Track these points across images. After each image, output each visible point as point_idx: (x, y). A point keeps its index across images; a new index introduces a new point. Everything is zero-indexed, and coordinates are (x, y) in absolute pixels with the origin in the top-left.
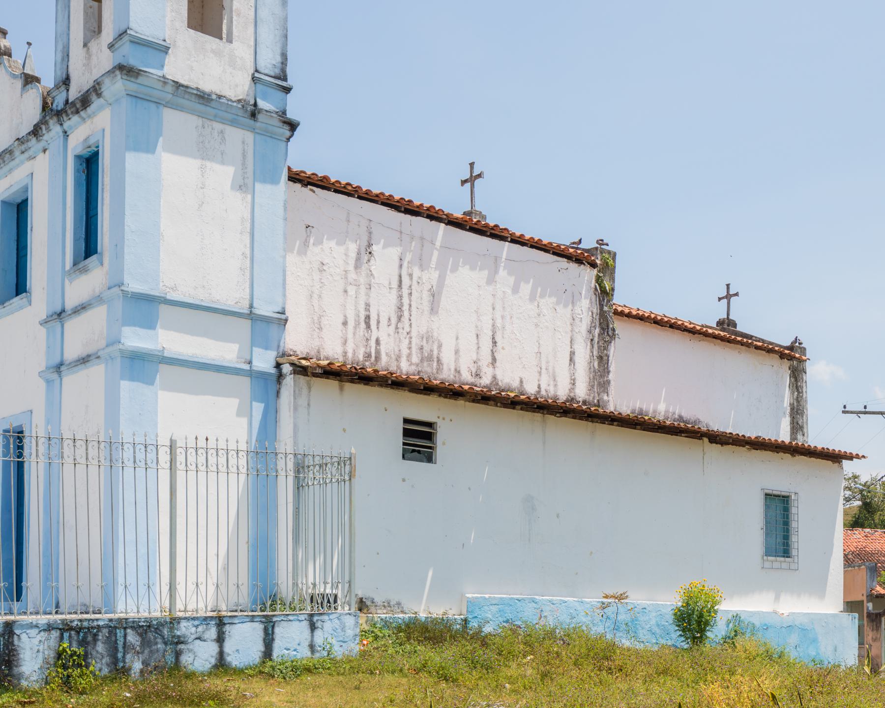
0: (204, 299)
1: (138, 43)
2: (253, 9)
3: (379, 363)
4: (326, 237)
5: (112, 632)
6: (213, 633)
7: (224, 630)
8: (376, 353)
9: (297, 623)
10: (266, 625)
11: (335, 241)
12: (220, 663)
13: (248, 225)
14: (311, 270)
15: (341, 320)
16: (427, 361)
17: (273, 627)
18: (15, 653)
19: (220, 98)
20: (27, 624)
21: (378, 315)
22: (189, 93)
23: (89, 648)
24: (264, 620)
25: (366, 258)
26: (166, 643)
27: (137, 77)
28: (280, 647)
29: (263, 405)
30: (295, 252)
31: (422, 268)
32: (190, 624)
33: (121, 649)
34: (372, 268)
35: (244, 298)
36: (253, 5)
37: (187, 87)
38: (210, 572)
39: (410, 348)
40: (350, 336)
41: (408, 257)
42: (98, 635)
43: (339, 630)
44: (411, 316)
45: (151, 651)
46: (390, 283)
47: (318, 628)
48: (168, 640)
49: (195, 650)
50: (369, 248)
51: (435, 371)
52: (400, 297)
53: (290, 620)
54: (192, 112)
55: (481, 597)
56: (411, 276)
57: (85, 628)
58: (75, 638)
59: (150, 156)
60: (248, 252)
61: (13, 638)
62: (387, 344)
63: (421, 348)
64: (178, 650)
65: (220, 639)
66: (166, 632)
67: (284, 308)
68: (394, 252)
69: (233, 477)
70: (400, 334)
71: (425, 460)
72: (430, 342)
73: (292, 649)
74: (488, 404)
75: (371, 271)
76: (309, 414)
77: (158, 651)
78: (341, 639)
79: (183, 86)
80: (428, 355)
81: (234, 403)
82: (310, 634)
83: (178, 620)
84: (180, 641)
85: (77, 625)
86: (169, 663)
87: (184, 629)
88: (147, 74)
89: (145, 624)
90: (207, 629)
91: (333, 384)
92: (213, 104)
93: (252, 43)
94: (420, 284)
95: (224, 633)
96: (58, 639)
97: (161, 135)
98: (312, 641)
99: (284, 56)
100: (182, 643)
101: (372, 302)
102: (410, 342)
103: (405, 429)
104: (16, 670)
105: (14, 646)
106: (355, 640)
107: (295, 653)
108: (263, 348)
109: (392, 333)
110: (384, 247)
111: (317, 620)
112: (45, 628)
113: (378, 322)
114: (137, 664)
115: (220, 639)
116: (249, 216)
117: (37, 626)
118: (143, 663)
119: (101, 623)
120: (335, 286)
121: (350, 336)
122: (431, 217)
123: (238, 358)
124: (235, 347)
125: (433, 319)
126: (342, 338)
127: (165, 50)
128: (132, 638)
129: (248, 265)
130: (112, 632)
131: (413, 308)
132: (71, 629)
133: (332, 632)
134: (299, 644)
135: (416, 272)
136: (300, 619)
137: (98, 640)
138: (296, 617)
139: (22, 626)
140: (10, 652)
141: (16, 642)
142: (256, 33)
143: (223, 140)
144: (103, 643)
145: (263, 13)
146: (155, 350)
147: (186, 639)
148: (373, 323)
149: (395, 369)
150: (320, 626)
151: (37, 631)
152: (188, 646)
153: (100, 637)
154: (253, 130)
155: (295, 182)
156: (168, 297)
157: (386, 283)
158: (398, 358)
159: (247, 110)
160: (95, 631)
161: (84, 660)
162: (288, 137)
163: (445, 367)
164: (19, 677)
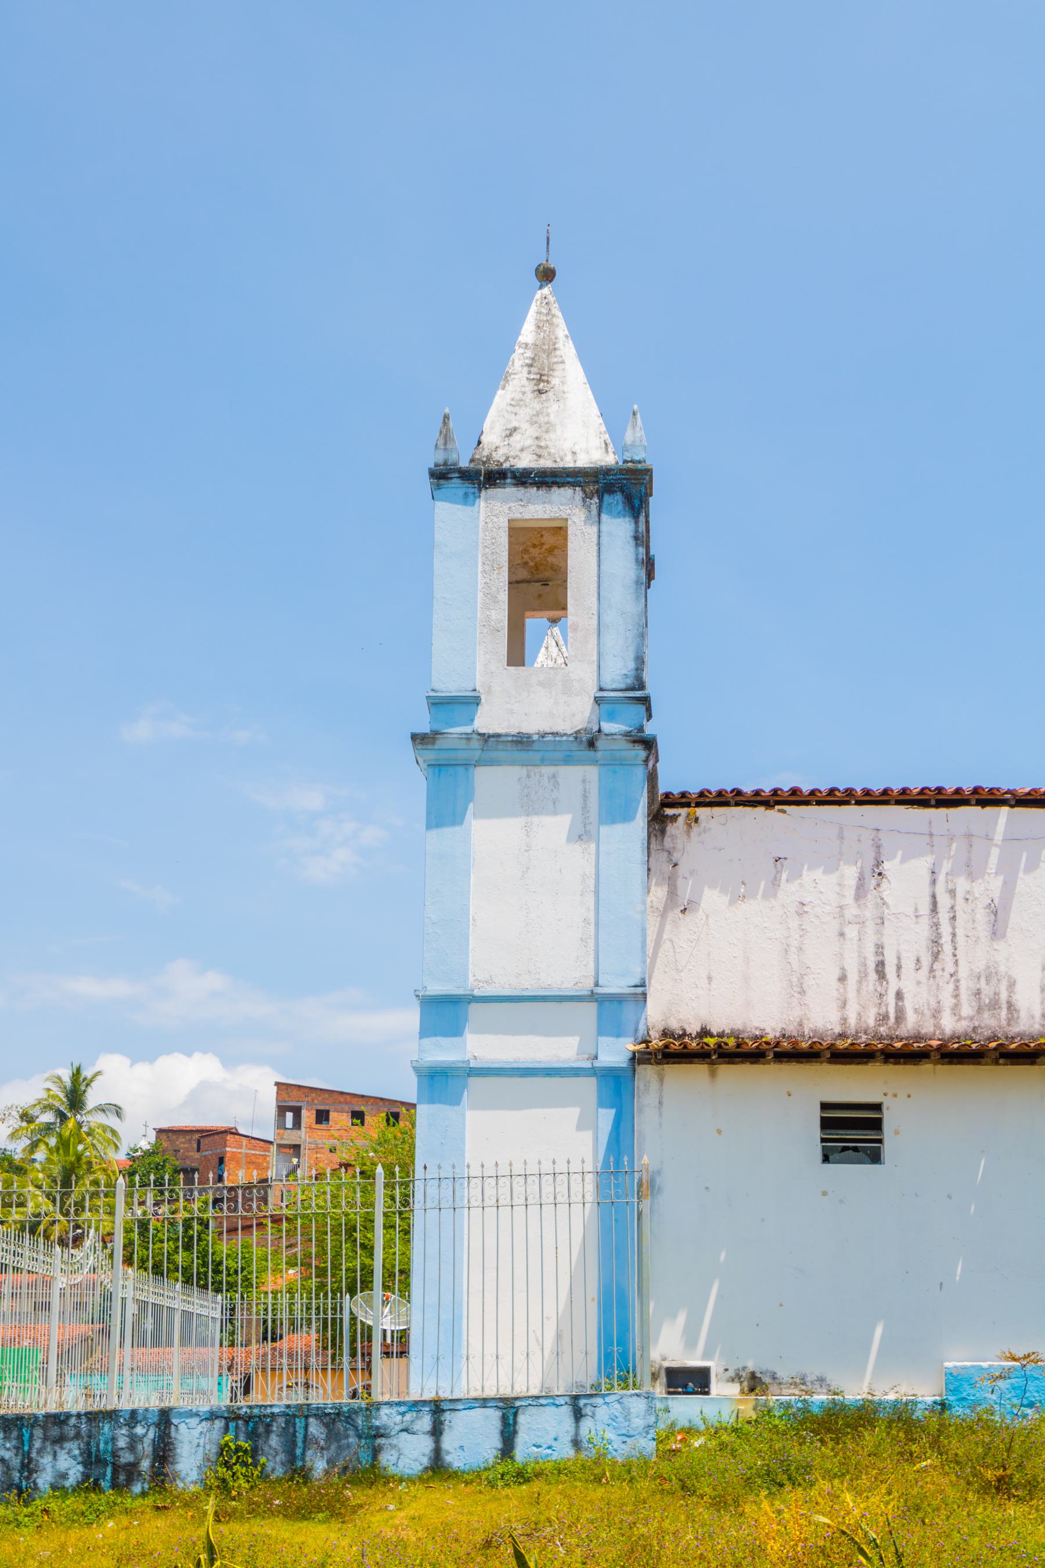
0: (529, 987)
1: (442, 704)
2: (596, 617)
3: (903, 1026)
4: (806, 867)
5: (290, 1421)
6: (425, 1422)
7: (443, 1419)
8: (896, 1012)
9: (553, 1408)
10: (505, 1411)
11: (821, 869)
12: (436, 1464)
13: (591, 883)
14: (785, 916)
15: (837, 973)
16: (989, 1010)
17: (515, 1415)
18: (171, 1447)
19: (543, 737)
20: (186, 1412)
21: (899, 958)
22: (502, 742)
23: (260, 1441)
24: (501, 1404)
25: (873, 882)
26: (360, 1437)
27: (434, 743)
28: (526, 1443)
29: (613, 1111)
30: (759, 897)
31: (971, 877)
32: (393, 1411)
33: (300, 1444)
34: (885, 895)
35: (586, 977)
36: (595, 612)
37: (499, 736)
38: (537, 1341)
39: (956, 996)
40: (851, 994)
41: (946, 866)
42: (272, 1426)
43: (621, 1419)
44: (956, 949)
45: (340, 1447)
46: (916, 909)
47: (586, 1415)
48: (363, 1433)
49: (400, 1446)
50: (878, 868)
51: (1004, 1023)
52: (936, 925)
53: (542, 1405)
54: (512, 763)
55: (973, 1367)
56: (952, 893)
57: (255, 1416)
58: (243, 1429)
59: (457, 829)
60: (591, 916)
61: (170, 1429)
62: (915, 996)
63: (978, 993)
64: (376, 1445)
65: (436, 1432)
66: (359, 1421)
67: (643, 979)
68: (922, 865)
69: (577, 1208)
70: (937, 978)
71: (867, 1159)
72: (994, 981)
73: (545, 1446)
74: (979, 1064)
75: (883, 899)
76: (661, 1115)
77: (348, 1446)
78: (624, 1432)
79: (490, 736)
80: (991, 1000)
81: (573, 1113)
82: (574, 1425)
83: (378, 1406)
84: (379, 1433)
85: (246, 1412)
86: (364, 1462)
87: (385, 1418)
88: (445, 735)
89: (332, 1411)
90: (417, 1418)
91: (699, 1071)
92: (536, 746)
93: (595, 658)
94: (970, 901)
95: (442, 1423)
96: (222, 1430)
97: (471, 800)
98: (577, 1434)
99: (640, 661)
100: (382, 1436)
101: (887, 941)
102: (957, 987)
103: (823, 1119)
104: (167, 1470)
105: (171, 1438)
106: (647, 1433)
107: (549, 1451)
108: (612, 1036)
109: (924, 980)
110: (903, 861)
111: (585, 1405)
112: (208, 1416)
113: (899, 968)
114: (320, 1463)
115: (436, 1432)
116: (593, 870)
117: (197, 1415)
118: (328, 1463)
119: (276, 1410)
120: (824, 930)
121: (851, 994)
122: (983, 803)
123: (578, 1054)
124: (574, 1041)
125: (996, 947)
126: (838, 999)
127: (476, 701)
128: (316, 1429)
129: (593, 933)
130: (290, 1421)
131: (960, 939)
132: (238, 1417)
133: (610, 1421)
134: (556, 1439)
135: (962, 885)
136: (557, 1402)
137: (272, 1432)
138: (551, 1401)
139: (181, 1415)
140: (165, 1446)
141: (173, 1434)
142: (599, 644)
143: (556, 785)
144: (277, 1435)
145: (608, 618)
146: (458, 1061)
147: (388, 1431)
148: (890, 970)
149: (932, 1029)
150: (590, 1413)
151: (197, 1420)
152: (390, 1441)
153: (274, 1429)
154: (595, 762)
155: (755, 806)
156: (476, 993)
157: (910, 911)
158: (936, 1013)
159: (581, 741)
160: (268, 1420)
161: (252, 1457)
162: (644, 759)
163: (1023, 1014)
164: (176, 1476)
